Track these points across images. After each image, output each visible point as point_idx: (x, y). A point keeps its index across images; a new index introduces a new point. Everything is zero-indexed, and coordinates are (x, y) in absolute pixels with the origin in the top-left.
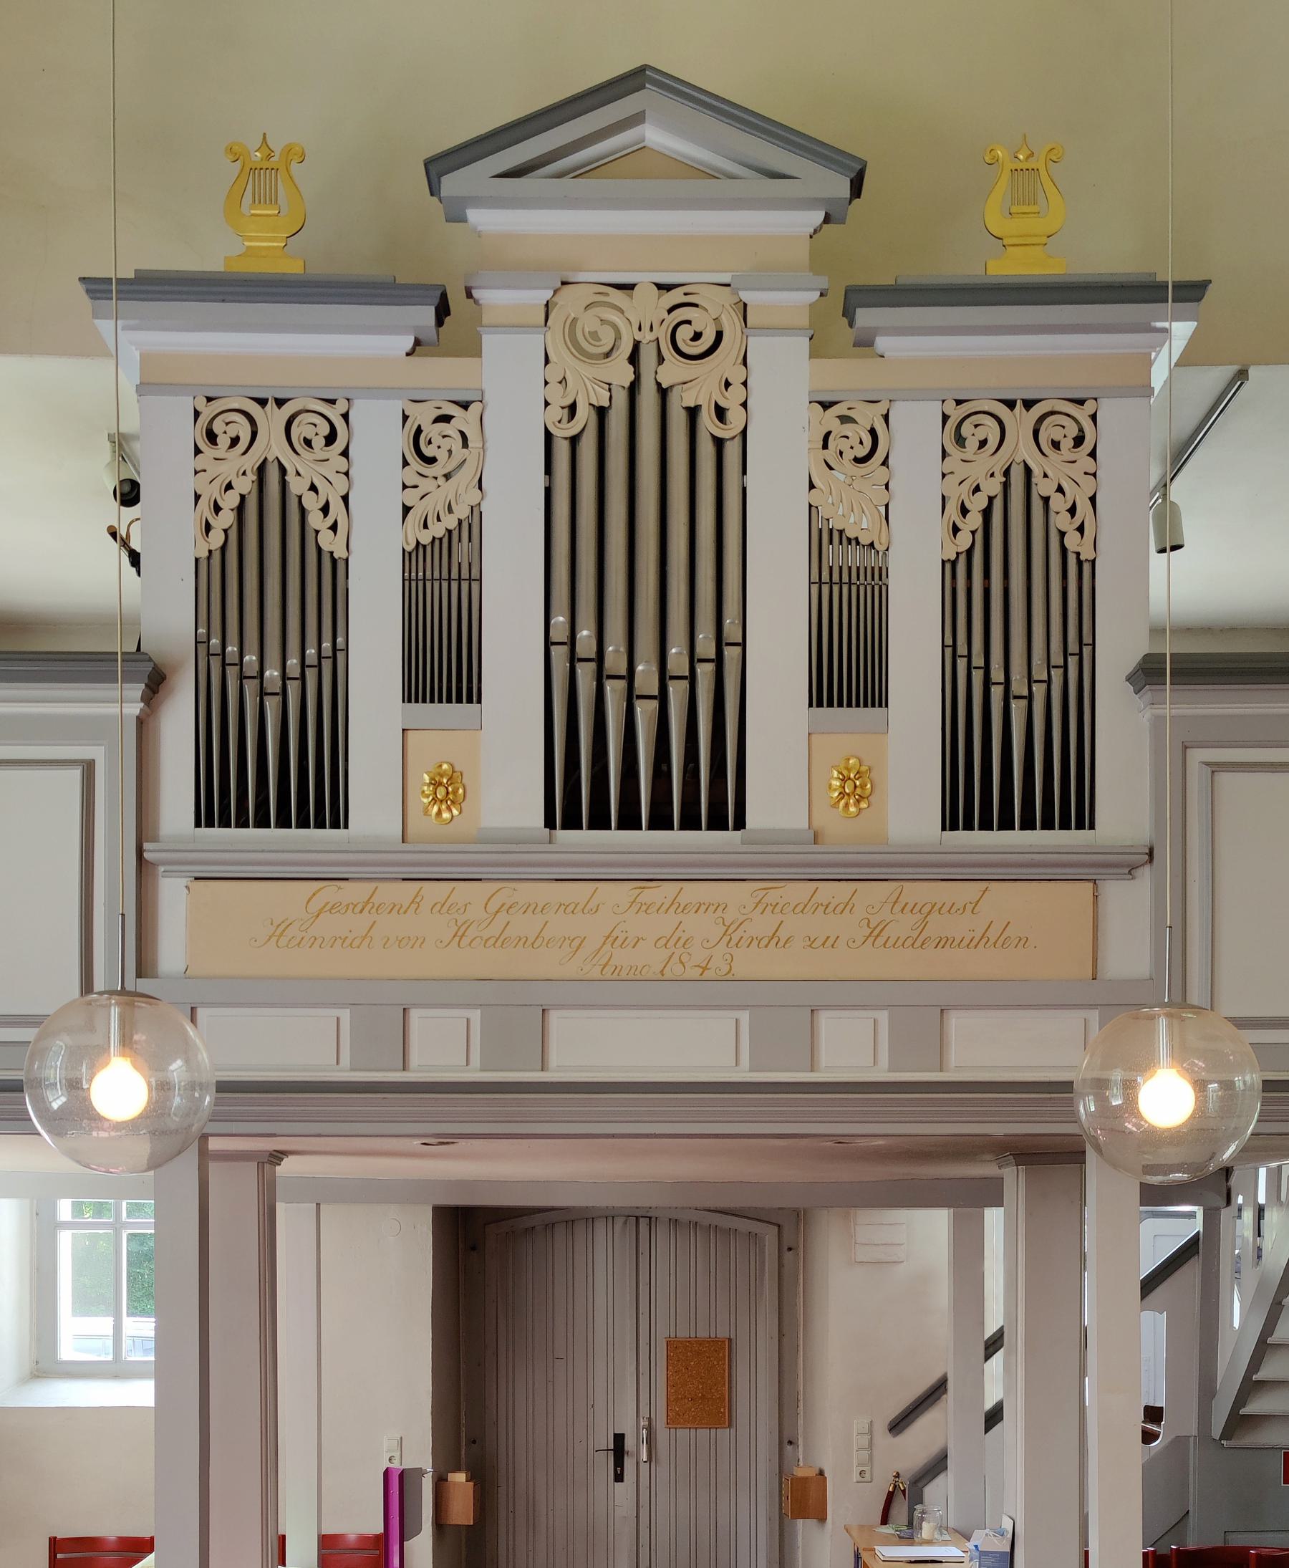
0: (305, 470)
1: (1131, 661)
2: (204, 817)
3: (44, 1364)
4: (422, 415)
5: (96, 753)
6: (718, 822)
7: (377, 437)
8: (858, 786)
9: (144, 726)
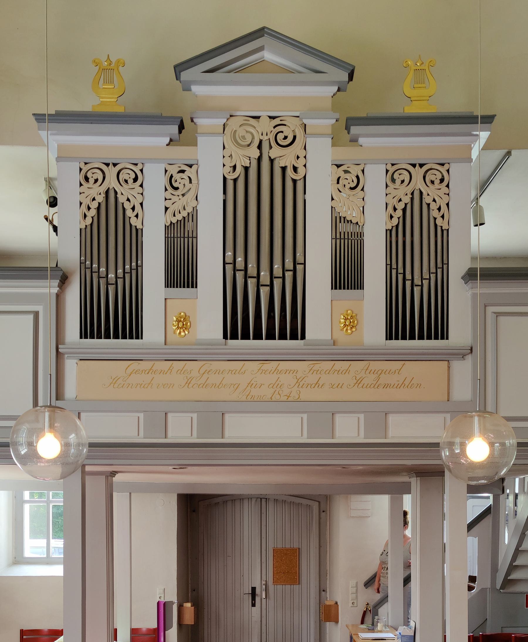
0: (125, 192)
1: (463, 271)
2: (84, 335)
3: (18, 558)
4: (173, 170)
5: (39, 308)
6: (294, 337)
7: (155, 179)
8: (352, 322)
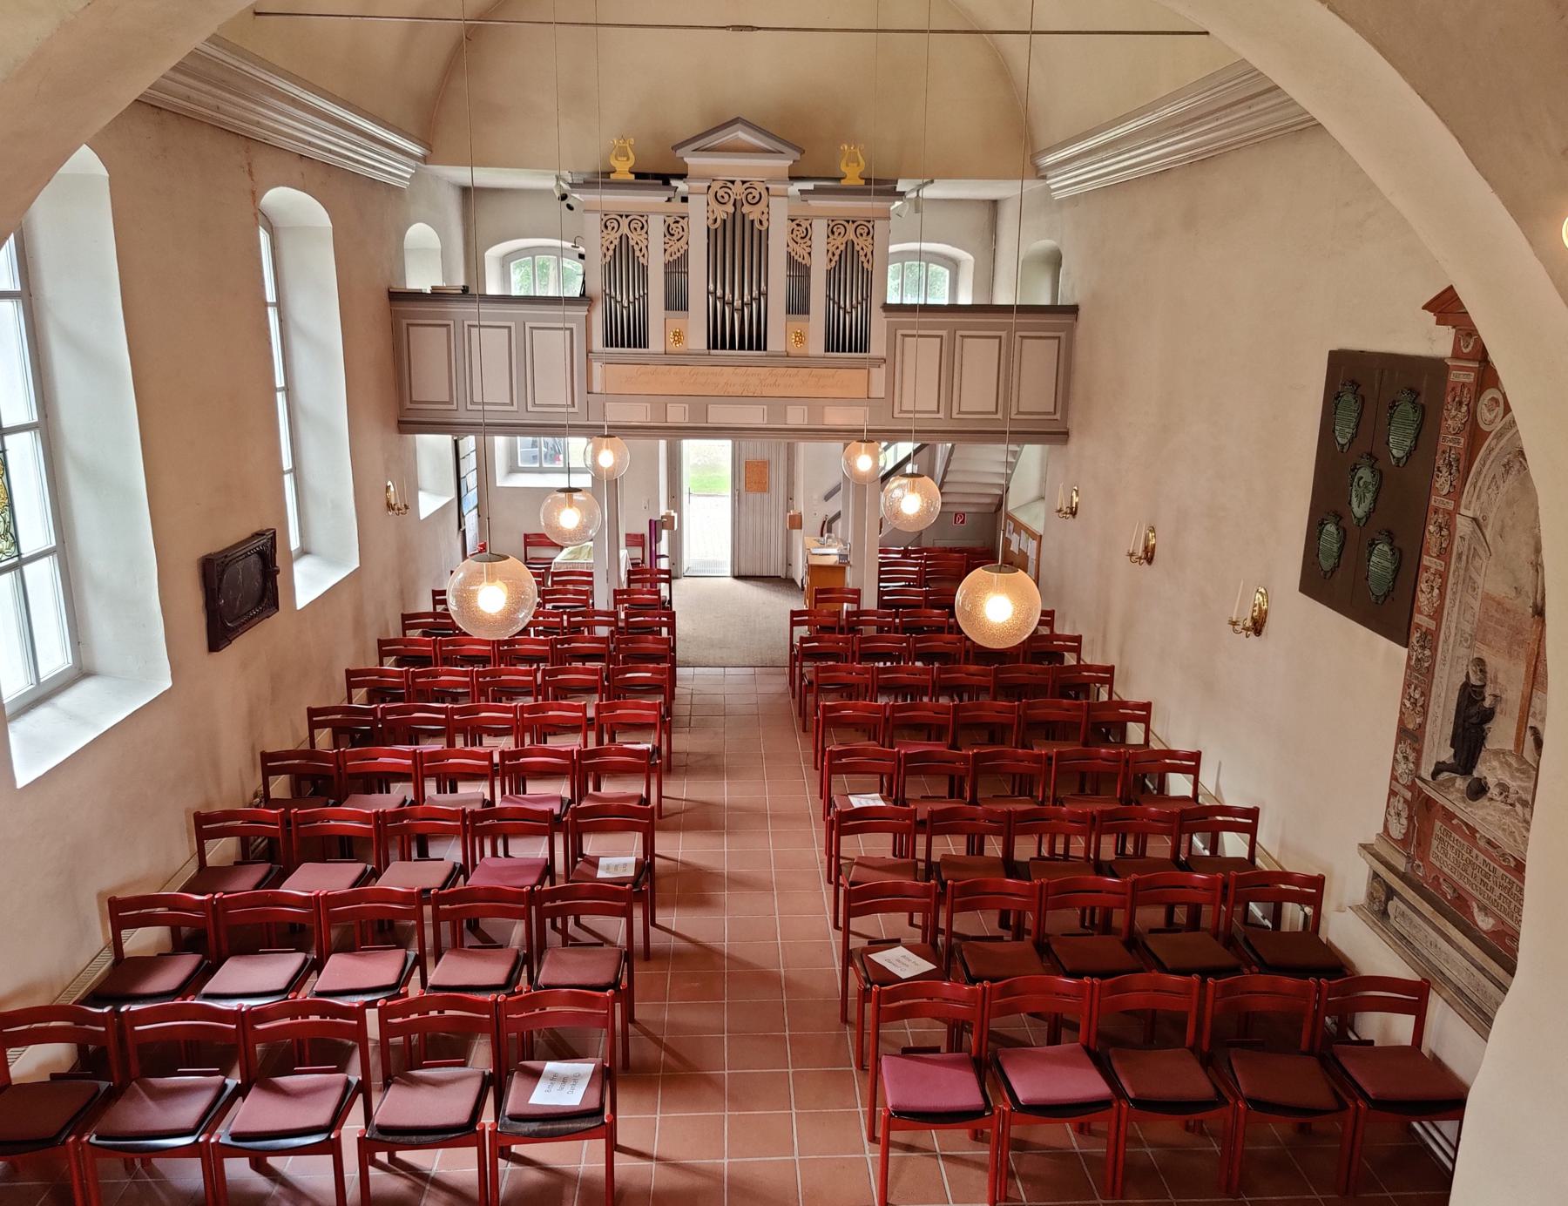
0: (634, 238)
4: (670, 221)
5: (573, 326)
6: (759, 348)
7: (656, 226)
8: (801, 338)
9: (588, 319)
